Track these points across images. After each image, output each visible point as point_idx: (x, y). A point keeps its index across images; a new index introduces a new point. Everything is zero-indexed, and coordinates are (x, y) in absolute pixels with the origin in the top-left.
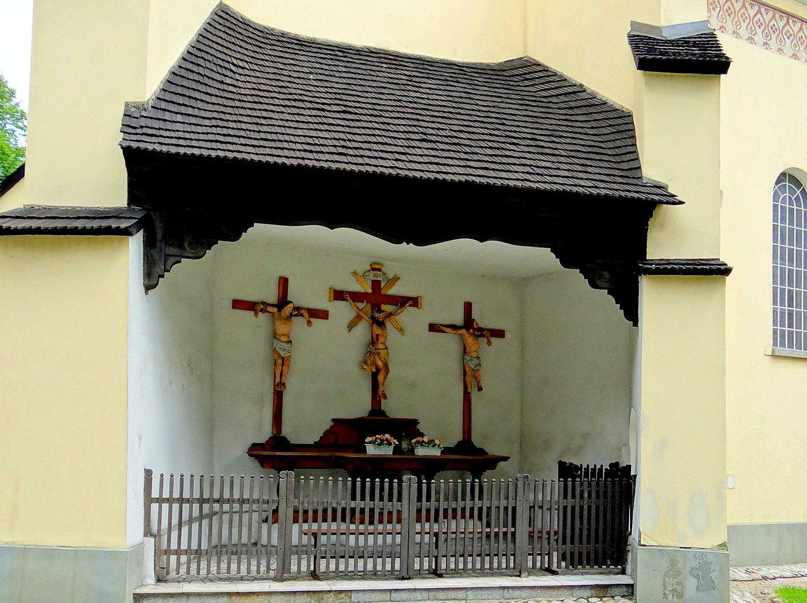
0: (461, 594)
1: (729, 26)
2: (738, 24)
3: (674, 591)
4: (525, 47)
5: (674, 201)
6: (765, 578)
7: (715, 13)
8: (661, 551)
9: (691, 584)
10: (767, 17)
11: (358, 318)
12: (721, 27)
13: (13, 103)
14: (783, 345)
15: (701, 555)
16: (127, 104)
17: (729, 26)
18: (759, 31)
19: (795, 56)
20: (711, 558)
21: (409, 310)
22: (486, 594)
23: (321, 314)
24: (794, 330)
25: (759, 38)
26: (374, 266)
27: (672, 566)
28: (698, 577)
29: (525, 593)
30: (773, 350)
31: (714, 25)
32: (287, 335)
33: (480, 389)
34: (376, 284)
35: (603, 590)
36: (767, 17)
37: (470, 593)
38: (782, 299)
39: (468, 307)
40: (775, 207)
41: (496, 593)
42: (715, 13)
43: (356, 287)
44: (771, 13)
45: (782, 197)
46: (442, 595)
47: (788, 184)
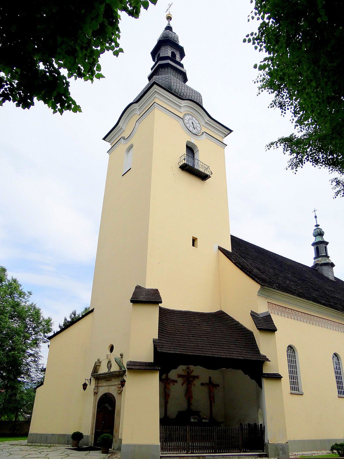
0: (229, 457)
1: (273, 312)
2: (275, 311)
3: (277, 455)
4: (221, 308)
5: (268, 360)
6: (295, 455)
7: (269, 309)
8: (273, 445)
9: (281, 452)
10: (281, 309)
11: (184, 382)
12: (271, 312)
13: (20, 289)
14: (293, 390)
15: (282, 445)
16: (153, 339)
17: (273, 312)
18: (279, 312)
19: (288, 317)
20: (284, 446)
21: (197, 380)
22: (235, 457)
23: (176, 381)
24: (295, 370)
25: (280, 314)
26: (188, 368)
27: (276, 448)
28: (282, 451)
29: (243, 456)
30: (291, 392)
31: (270, 312)
32: (169, 388)
33: (214, 402)
34: (188, 373)
35: (260, 456)
36: (281, 309)
37: (231, 456)
38: (291, 373)
39: (210, 378)
40: (287, 354)
41: (237, 456)
42: (269, 309)
43: (183, 374)
44: (282, 307)
45: (288, 351)
46: (225, 457)
47: (289, 348)
